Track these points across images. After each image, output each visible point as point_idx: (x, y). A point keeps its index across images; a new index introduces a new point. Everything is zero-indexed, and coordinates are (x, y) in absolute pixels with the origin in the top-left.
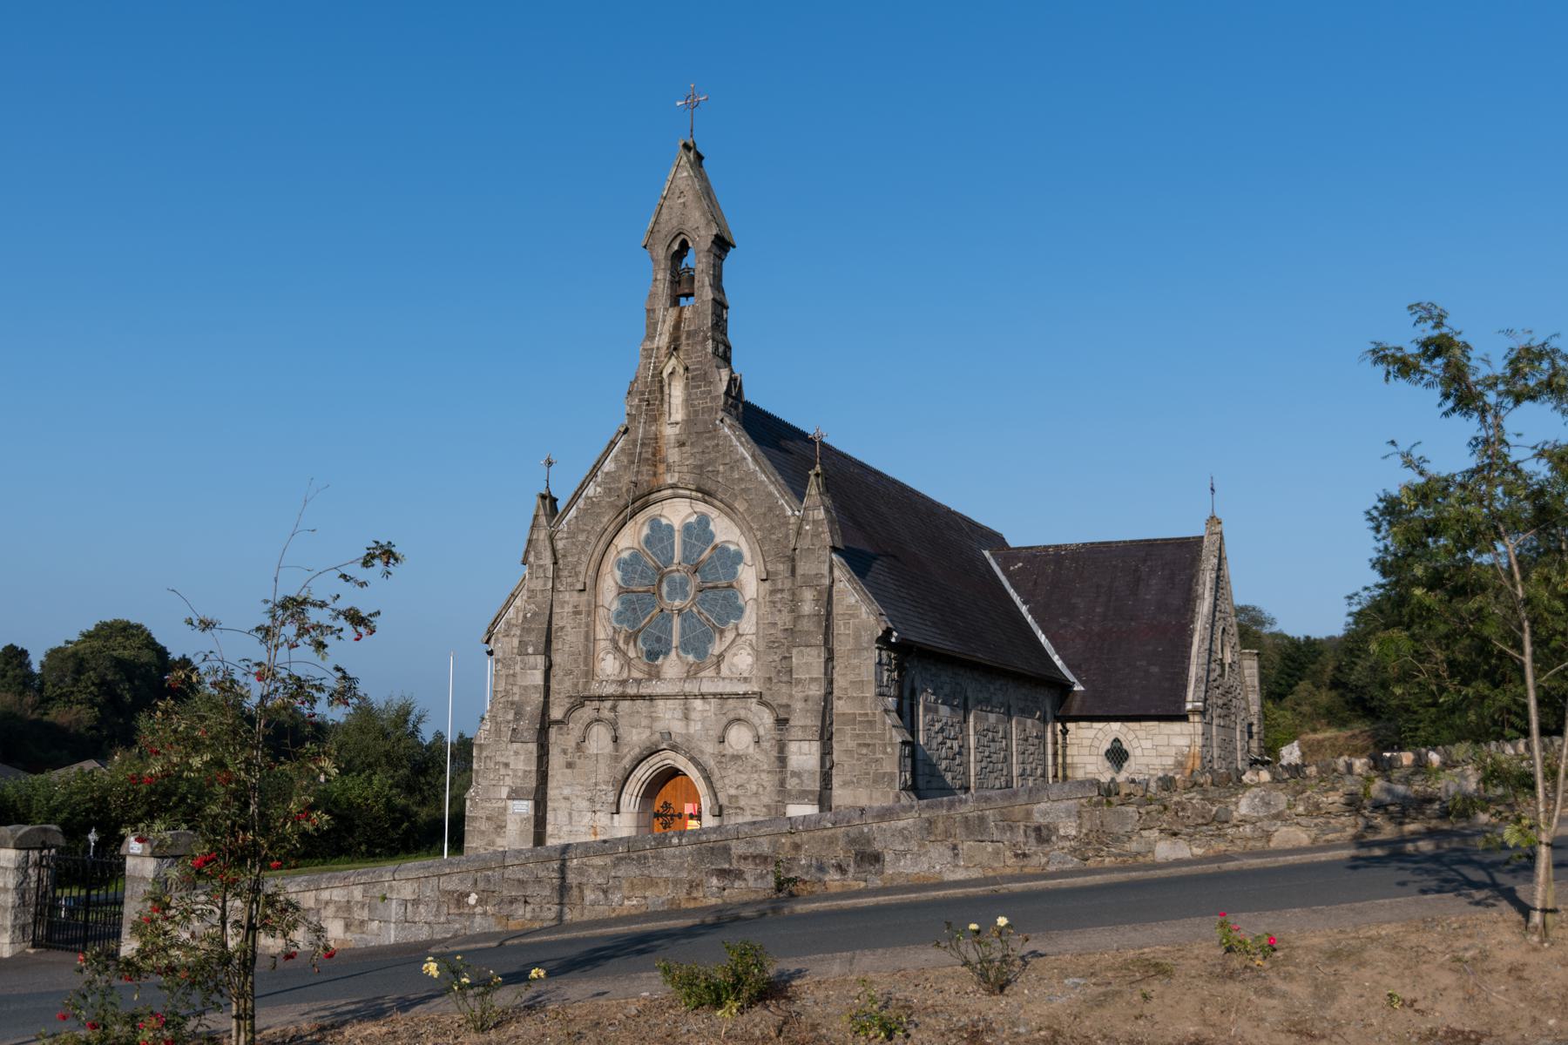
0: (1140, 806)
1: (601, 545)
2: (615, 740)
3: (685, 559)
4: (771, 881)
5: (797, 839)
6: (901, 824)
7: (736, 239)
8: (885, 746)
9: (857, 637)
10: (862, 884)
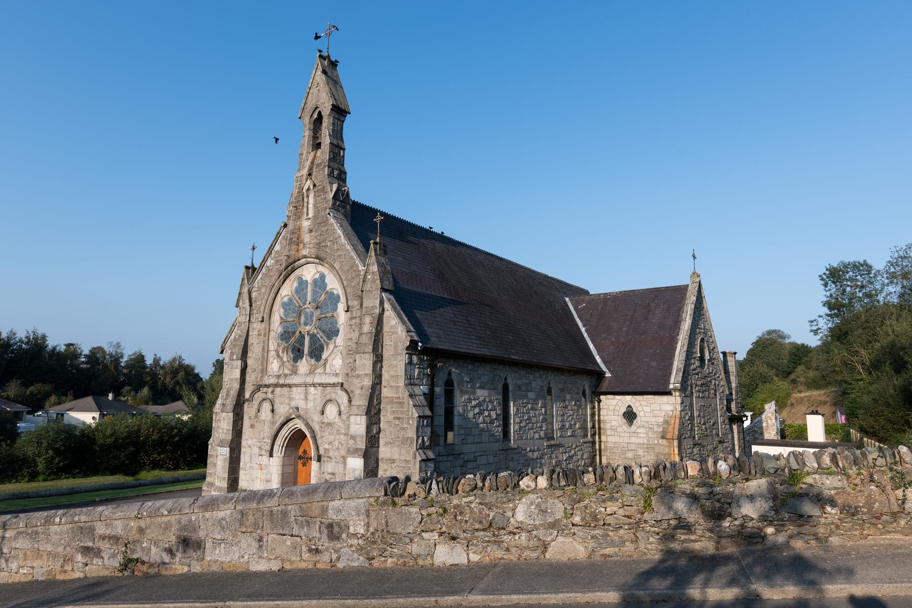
0: (421, 508)
1: (272, 295)
2: (273, 411)
3: (314, 300)
4: (120, 558)
5: (142, 523)
6: (221, 514)
7: (351, 108)
8: (408, 419)
9: (396, 347)
10: (186, 569)
